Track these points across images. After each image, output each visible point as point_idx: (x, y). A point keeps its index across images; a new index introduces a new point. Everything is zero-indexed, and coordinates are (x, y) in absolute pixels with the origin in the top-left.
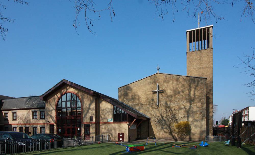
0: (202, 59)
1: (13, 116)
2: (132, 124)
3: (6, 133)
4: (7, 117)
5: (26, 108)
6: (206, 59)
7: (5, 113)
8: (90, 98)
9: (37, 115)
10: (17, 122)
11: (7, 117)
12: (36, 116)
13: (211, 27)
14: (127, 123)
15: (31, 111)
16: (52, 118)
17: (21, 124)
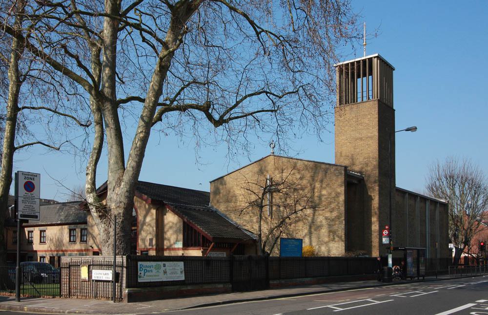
0: (360, 122)
1: (41, 237)
2: (210, 251)
3: (30, 264)
4: (31, 237)
5: (59, 222)
6: (366, 121)
7: (29, 232)
8: (145, 207)
9: (75, 236)
10: (45, 247)
11: (31, 237)
12: (74, 237)
13: (375, 57)
14: (200, 249)
15: (66, 229)
16: (94, 239)
17: (51, 251)
